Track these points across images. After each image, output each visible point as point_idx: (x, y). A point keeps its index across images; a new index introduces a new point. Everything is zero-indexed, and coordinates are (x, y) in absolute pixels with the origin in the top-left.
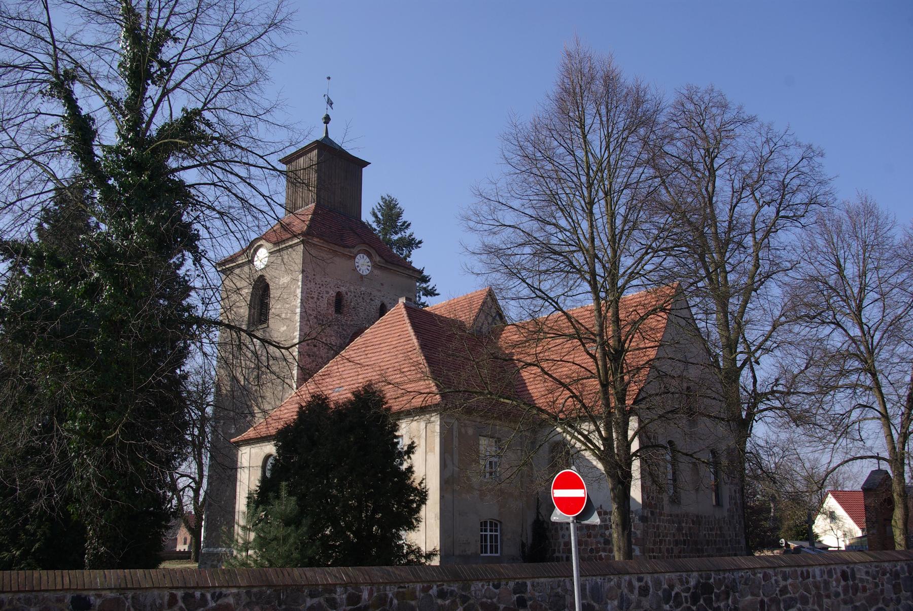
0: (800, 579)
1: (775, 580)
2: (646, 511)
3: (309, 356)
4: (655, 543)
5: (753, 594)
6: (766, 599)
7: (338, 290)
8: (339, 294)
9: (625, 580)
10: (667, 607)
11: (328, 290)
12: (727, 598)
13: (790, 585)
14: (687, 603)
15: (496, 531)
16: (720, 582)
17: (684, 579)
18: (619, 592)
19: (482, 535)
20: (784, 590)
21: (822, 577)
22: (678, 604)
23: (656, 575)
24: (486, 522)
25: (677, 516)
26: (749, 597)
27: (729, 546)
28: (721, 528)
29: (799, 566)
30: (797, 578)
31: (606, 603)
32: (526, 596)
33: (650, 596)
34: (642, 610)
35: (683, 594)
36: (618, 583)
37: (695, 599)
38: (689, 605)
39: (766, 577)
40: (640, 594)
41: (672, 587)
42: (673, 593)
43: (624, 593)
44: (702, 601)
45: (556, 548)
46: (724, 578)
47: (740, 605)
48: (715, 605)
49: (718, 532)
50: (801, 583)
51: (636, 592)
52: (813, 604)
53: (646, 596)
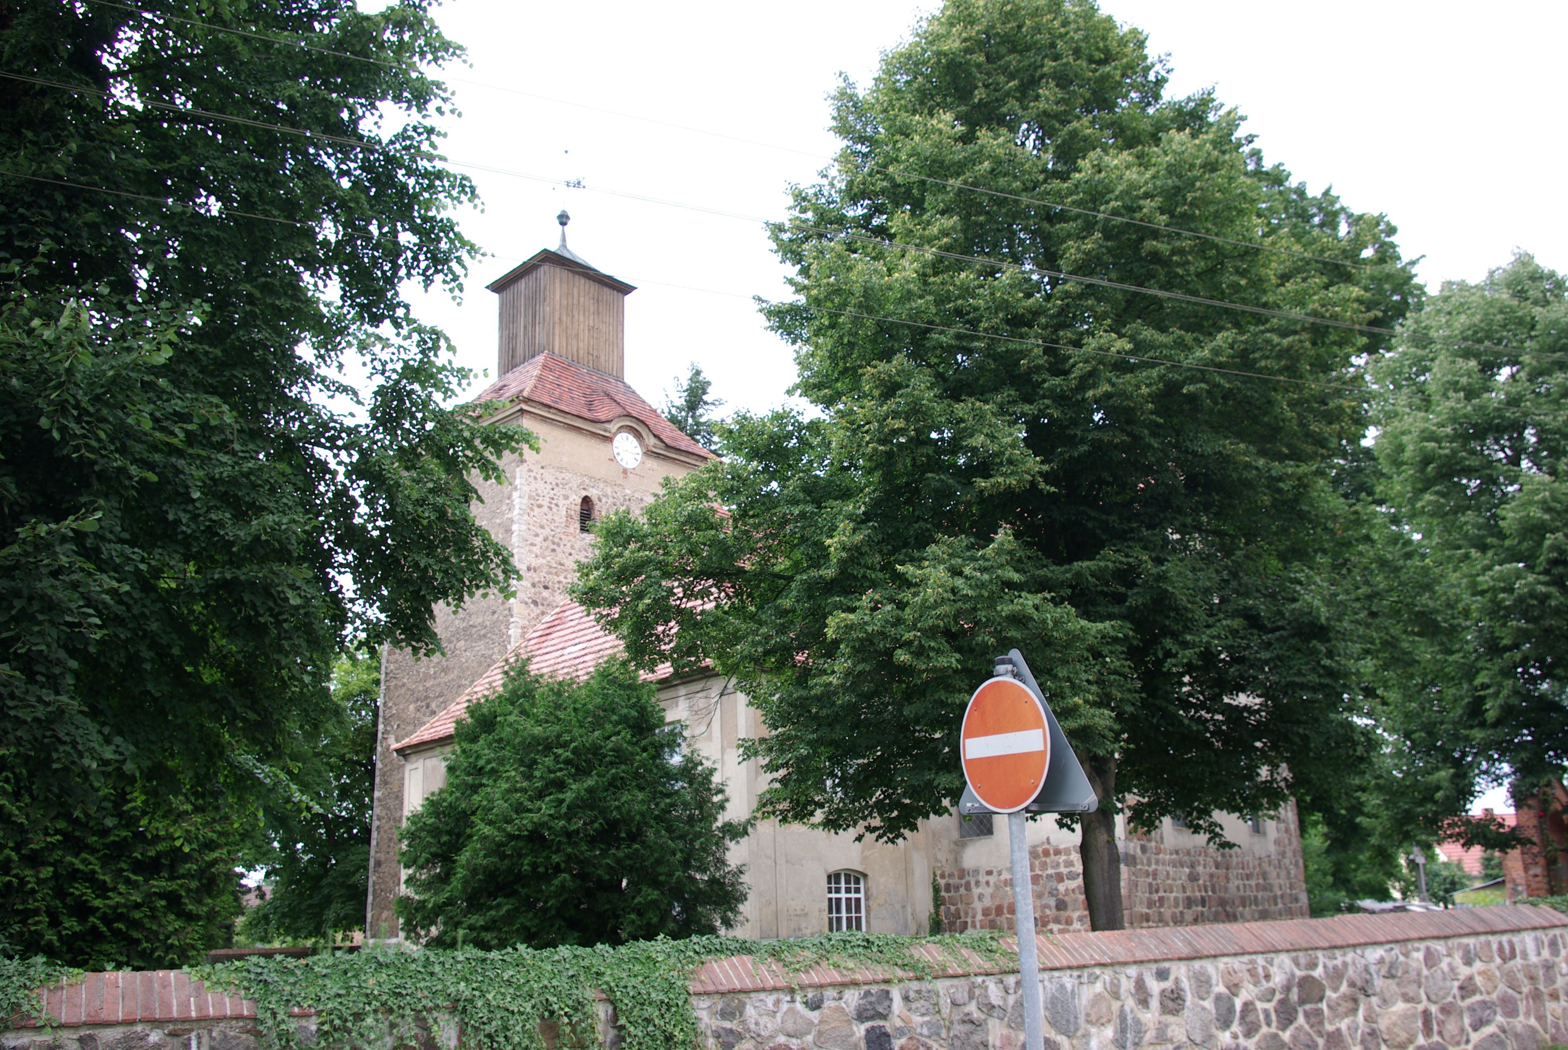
0: (1498, 961)
1: (1450, 965)
2: (1132, 845)
3: (535, 603)
4: (1150, 904)
5: (1407, 999)
6: (1434, 1009)
7: (584, 493)
8: (586, 501)
9: (1128, 977)
10: (1225, 1037)
11: (568, 492)
12: (1355, 1010)
13: (1480, 973)
14: (1269, 1024)
15: (857, 891)
16: (1336, 975)
17: (1260, 971)
18: (1116, 1006)
19: (830, 900)
20: (1467, 989)
21: (1539, 954)
22: (1250, 1031)
23: (1197, 965)
24: (837, 876)
25: (1188, 853)
26: (1400, 1006)
27: (1280, 905)
28: (1264, 875)
29: (1493, 933)
30: (1491, 959)
31: (1087, 1036)
32: (888, 1026)
33: (1186, 1012)
34: (1170, 1047)
35: (1260, 1005)
36: (1112, 983)
37: (1286, 1014)
38: (1273, 1029)
39: (1431, 959)
40: (1165, 1010)
41: (1234, 988)
42: (1238, 1003)
43: (1127, 1009)
44: (1301, 1020)
45: (969, 920)
46: (1345, 964)
47: (1383, 1024)
48: (1329, 1028)
49: (1261, 881)
50: (1498, 968)
51: (1155, 1003)
52: (1527, 1014)
53: (1175, 1012)
